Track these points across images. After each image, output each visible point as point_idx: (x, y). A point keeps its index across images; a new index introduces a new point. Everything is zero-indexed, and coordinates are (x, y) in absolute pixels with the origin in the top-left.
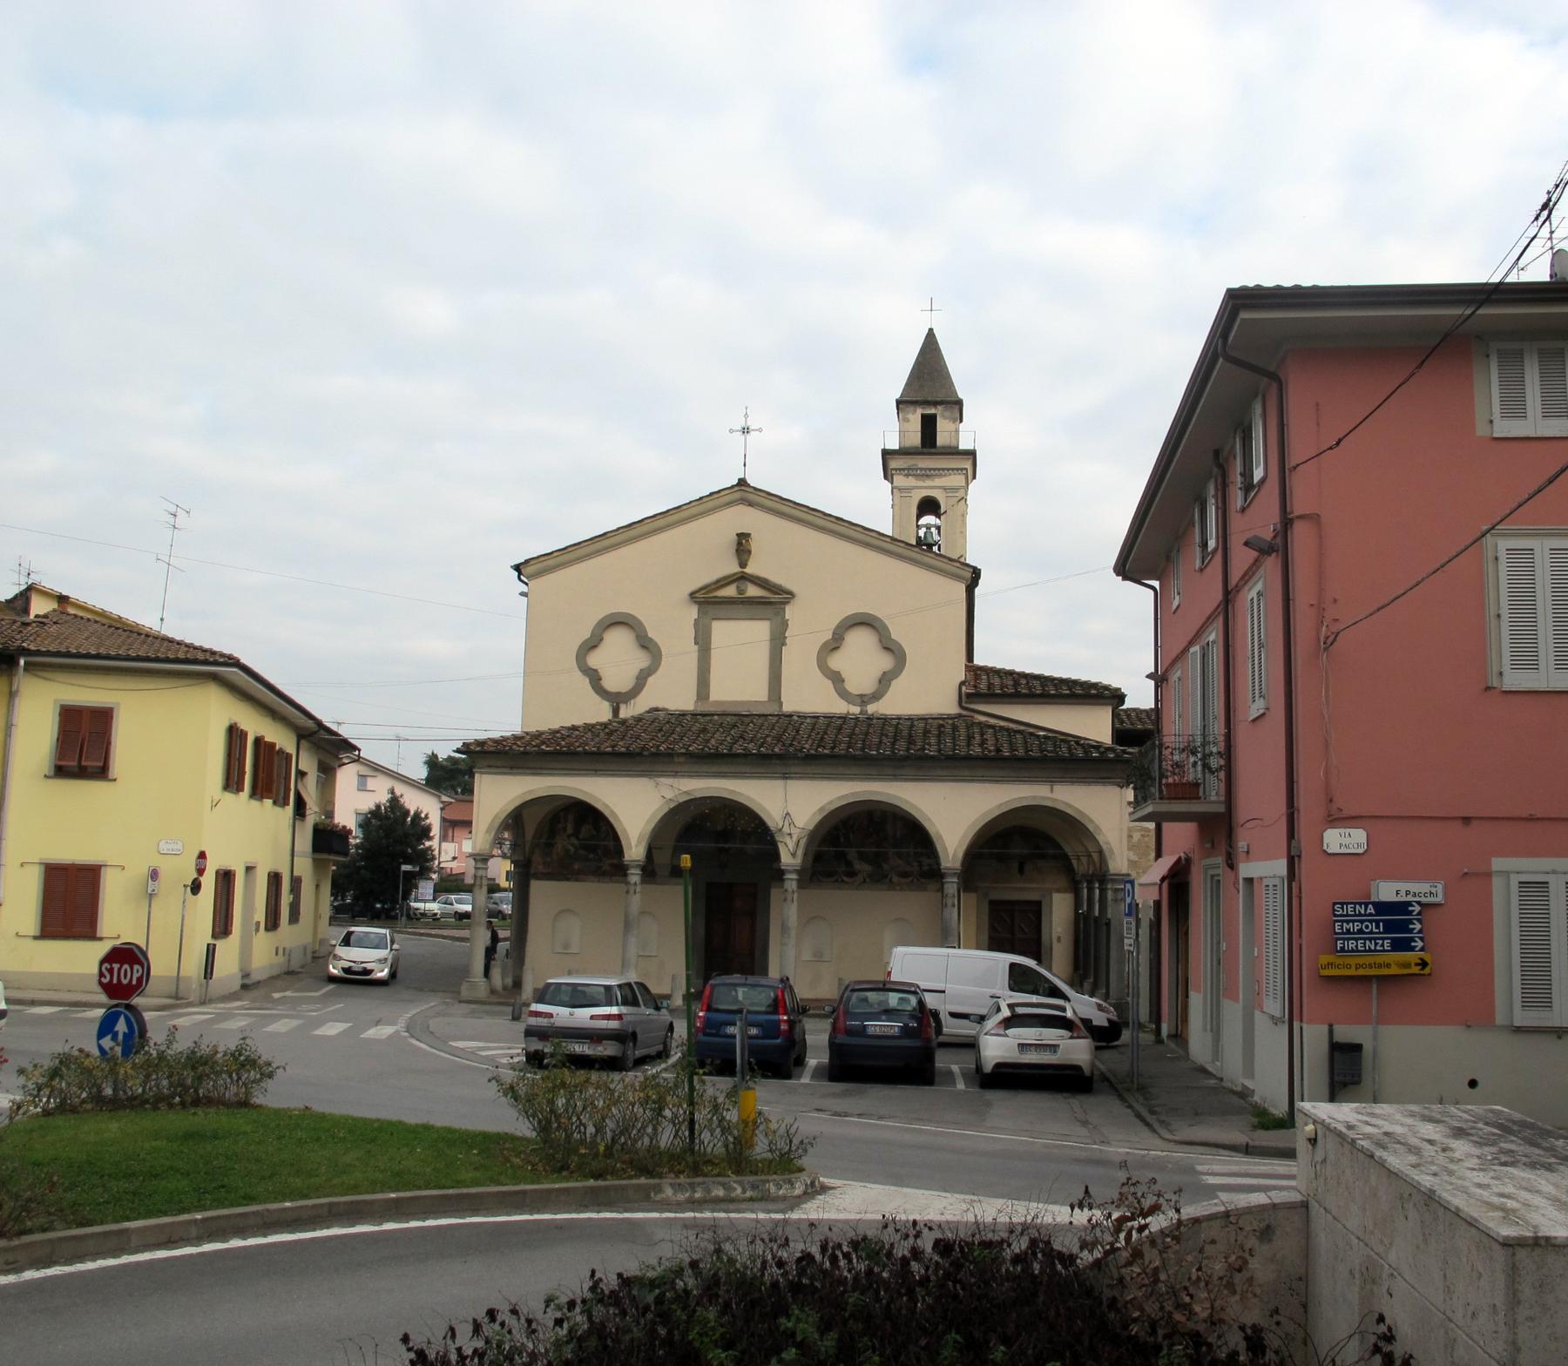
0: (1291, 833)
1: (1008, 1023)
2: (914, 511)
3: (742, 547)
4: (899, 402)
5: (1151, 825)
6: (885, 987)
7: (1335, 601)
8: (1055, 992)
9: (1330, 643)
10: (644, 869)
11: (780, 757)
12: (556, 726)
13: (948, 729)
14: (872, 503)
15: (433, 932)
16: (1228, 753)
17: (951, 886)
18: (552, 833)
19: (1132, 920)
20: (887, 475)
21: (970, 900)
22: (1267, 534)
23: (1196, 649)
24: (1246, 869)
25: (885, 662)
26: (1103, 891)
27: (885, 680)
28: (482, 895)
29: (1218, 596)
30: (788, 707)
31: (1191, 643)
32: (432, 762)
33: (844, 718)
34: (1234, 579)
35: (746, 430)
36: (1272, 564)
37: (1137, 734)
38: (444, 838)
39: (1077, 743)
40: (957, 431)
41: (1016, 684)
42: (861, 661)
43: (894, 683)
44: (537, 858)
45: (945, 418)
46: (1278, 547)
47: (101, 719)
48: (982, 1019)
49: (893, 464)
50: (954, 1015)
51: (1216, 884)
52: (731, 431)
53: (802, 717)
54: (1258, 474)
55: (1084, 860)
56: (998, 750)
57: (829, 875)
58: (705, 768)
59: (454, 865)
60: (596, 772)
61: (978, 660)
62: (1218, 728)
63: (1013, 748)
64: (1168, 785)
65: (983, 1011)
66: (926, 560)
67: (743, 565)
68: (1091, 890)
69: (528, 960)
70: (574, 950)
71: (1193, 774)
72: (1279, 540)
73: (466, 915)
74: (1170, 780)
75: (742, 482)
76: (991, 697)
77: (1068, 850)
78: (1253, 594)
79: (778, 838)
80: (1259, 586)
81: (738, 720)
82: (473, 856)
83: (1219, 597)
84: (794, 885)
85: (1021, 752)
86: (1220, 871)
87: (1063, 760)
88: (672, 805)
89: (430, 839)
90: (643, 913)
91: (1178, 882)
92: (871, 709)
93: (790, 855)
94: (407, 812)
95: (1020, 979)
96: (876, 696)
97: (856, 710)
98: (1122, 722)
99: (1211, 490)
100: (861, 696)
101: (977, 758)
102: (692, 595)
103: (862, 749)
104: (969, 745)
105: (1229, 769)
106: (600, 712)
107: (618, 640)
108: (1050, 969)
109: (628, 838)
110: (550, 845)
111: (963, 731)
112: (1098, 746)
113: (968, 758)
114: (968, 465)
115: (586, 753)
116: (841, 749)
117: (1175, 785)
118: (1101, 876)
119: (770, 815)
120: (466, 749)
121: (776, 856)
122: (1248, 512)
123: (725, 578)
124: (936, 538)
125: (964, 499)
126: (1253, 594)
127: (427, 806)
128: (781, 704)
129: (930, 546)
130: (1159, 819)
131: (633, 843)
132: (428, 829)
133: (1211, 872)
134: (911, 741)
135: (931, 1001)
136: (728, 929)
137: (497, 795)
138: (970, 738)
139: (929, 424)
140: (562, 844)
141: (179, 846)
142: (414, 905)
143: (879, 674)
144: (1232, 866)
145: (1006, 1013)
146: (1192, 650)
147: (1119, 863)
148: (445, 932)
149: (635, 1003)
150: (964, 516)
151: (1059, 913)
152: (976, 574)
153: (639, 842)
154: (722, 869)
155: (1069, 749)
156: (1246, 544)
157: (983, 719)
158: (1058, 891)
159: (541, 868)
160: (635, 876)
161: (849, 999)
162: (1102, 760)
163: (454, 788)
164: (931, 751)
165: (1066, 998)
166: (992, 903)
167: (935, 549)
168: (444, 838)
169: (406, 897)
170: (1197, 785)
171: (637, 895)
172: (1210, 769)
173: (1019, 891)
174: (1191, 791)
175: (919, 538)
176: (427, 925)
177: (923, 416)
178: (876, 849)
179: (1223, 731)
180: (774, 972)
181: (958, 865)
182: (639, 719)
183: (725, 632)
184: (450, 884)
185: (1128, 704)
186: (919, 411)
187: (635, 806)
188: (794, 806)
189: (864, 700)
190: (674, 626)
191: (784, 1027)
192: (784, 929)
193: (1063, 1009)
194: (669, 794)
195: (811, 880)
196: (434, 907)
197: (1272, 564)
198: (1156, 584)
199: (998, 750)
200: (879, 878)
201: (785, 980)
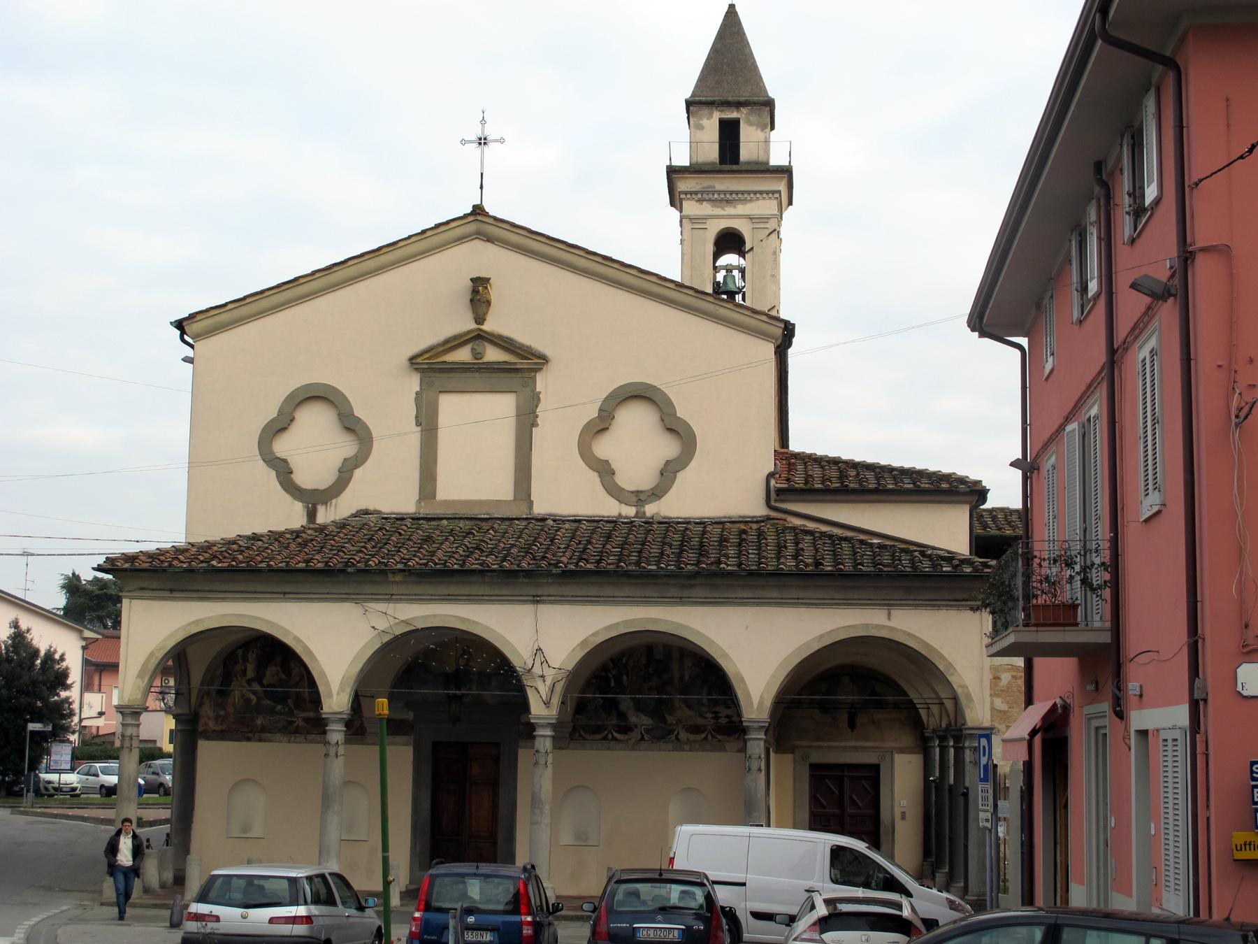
0: (1194, 670)
1: (824, 924)
2: (710, 248)
3: (479, 294)
4: (689, 104)
5: (1019, 662)
6: (662, 877)
7: (1251, 361)
8: (891, 884)
9: (1243, 417)
10: (348, 724)
11: (528, 574)
12: (231, 534)
13: (752, 537)
14: (656, 239)
15: (70, 812)
16: (1115, 566)
17: (756, 746)
18: (227, 678)
19: (989, 786)
20: (675, 201)
21: (782, 765)
22: (1162, 273)
23: (1073, 427)
24: (1139, 719)
25: (668, 448)
26: (959, 751)
27: (669, 472)
28: (131, 760)
29: (1101, 357)
30: (539, 509)
31: (1067, 420)
32: (73, 586)
33: (614, 522)
34: (1121, 332)
35: (482, 141)
36: (1168, 311)
37: (999, 541)
38: (87, 686)
39: (923, 554)
40: (767, 142)
41: (842, 476)
42: (636, 447)
43: (680, 475)
44: (207, 711)
45: (750, 123)
46: (1175, 290)
48: (792, 919)
49: (683, 185)
50: (757, 915)
51: (1101, 737)
53: (559, 520)
54: (1151, 193)
55: (935, 709)
56: (818, 564)
57: (596, 730)
58: (429, 589)
59: (100, 722)
60: (285, 596)
61: (795, 446)
62: (1102, 532)
63: (837, 563)
64: (1037, 607)
65: (793, 910)
66: (723, 312)
67: (480, 319)
68: (943, 749)
69: (195, 845)
70: (257, 831)
71: (1072, 592)
72: (1176, 281)
73: (110, 791)
74: (1040, 601)
75: (478, 210)
76: (808, 493)
77: (913, 695)
78: (1145, 353)
79: (527, 681)
80: (1153, 343)
81: (474, 525)
82: (121, 709)
83: (1103, 358)
84: (548, 744)
85: (848, 567)
86: (1106, 722)
87: (903, 576)
88: (386, 639)
89: (67, 687)
90: (347, 783)
91: (1053, 738)
92: (650, 510)
93: (543, 704)
94: (36, 653)
95: (845, 866)
96: (657, 493)
97: (630, 511)
98: (985, 526)
99: (1092, 215)
100: (637, 493)
101: (790, 575)
102: (412, 360)
103: (638, 563)
104: (778, 557)
105: (1116, 584)
106: (291, 516)
107: (315, 420)
108: (891, 857)
109: (327, 683)
110: (222, 693)
111: (771, 539)
112: (950, 557)
113: (777, 574)
114: (782, 186)
115: (272, 571)
116: (610, 563)
117: (1045, 606)
118: (956, 733)
119: (516, 651)
120: (110, 565)
121: (523, 705)
122: (1138, 242)
123: (455, 337)
124: (739, 283)
125: (776, 232)
126: (1145, 353)
127: (64, 645)
128: (531, 504)
129: (732, 295)
130: (1029, 652)
131: (335, 687)
132: (64, 674)
133: (1095, 723)
134: (702, 551)
135: (724, 896)
136: (463, 808)
137: (152, 627)
138: (780, 547)
139: (729, 133)
140: (239, 692)
142: (45, 776)
144: (1120, 715)
145: (822, 910)
146: (1069, 428)
147: (978, 713)
148: (86, 813)
149: (330, 901)
150: (776, 254)
151: (903, 781)
152: (788, 331)
153: (342, 689)
154: (453, 721)
155: (912, 561)
156: (1134, 286)
157: (797, 522)
158: (902, 751)
159: (212, 725)
160: (336, 734)
161: (613, 895)
162: (955, 577)
163: (101, 619)
164: (730, 565)
165: (909, 894)
166: (813, 767)
167: (739, 298)
168: (87, 686)
169: (34, 766)
170: (1074, 607)
171: (339, 759)
172: (1091, 586)
173: (850, 751)
174: (1066, 615)
175: (716, 285)
176: (62, 804)
178: (652, 695)
179: (1109, 535)
180: (521, 859)
181: (765, 715)
182: (342, 525)
183: (455, 409)
184: (95, 749)
185: (988, 505)
186: (717, 115)
187: (336, 640)
188: (547, 639)
189: (640, 498)
190: (389, 403)
191: (527, 931)
192: (535, 803)
193: (899, 906)
194: (382, 624)
195: (572, 737)
196: (72, 779)
197: (1168, 311)
198: (1024, 341)
199: (818, 564)
200: (662, 734)
201: (530, 870)
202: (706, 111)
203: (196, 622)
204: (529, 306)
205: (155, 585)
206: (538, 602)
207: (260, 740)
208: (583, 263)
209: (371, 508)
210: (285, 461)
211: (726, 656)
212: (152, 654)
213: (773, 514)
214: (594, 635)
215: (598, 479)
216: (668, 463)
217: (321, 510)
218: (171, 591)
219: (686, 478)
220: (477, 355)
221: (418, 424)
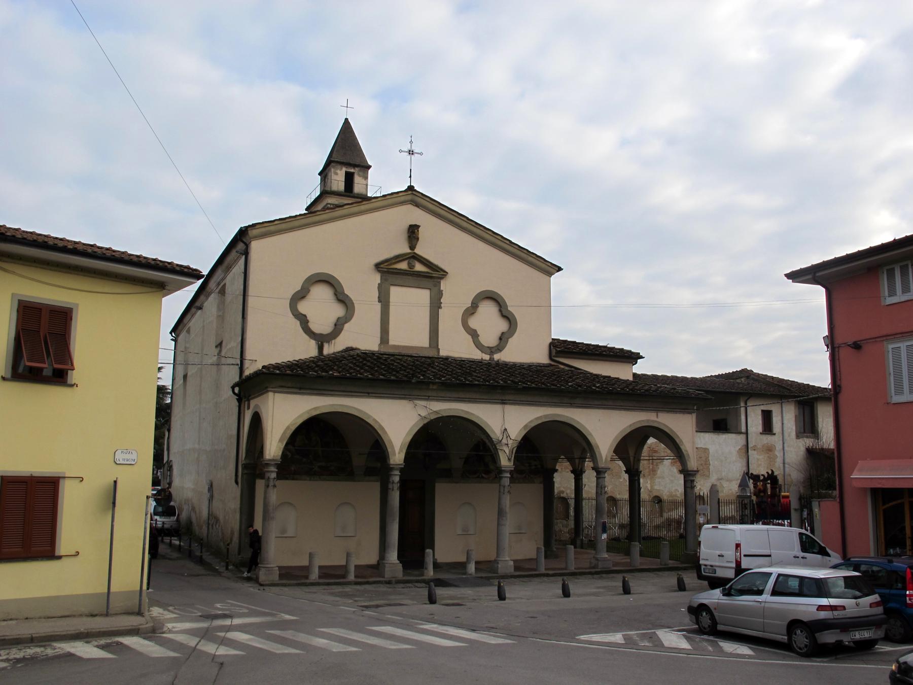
3: (413, 232)
25: (503, 326)
27: (503, 339)
30: (443, 353)
43: (510, 340)
45: (359, 176)
47: (61, 318)
52: (401, 151)
60: (369, 395)
67: (412, 247)
75: (411, 188)
88: (426, 422)
92: (496, 357)
93: (505, 460)
96: (499, 348)
97: (486, 357)
102: (378, 266)
109: (393, 447)
119: (492, 430)
128: (438, 350)
131: (397, 449)
139: (349, 178)
141: (134, 456)
143: (499, 334)
177: (346, 173)
183: (397, 293)
186: (344, 169)
189: (491, 351)
190: (363, 287)
202: (339, 167)
203: (315, 409)
204: (437, 243)
205: (289, 385)
206: (504, 403)
207: (293, 479)
208: (465, 224)
209: (354, 346)
210: (305, 316)
211: (591, 434)
212: (288, 428)
213: (553, 363)
214: (531, 422)
215: (471, 340)
216: (503, 333)
217: (326, 346)
218: (300, 389)
219: (512, 342)
220: (411, 266)
221: (380, 301)
